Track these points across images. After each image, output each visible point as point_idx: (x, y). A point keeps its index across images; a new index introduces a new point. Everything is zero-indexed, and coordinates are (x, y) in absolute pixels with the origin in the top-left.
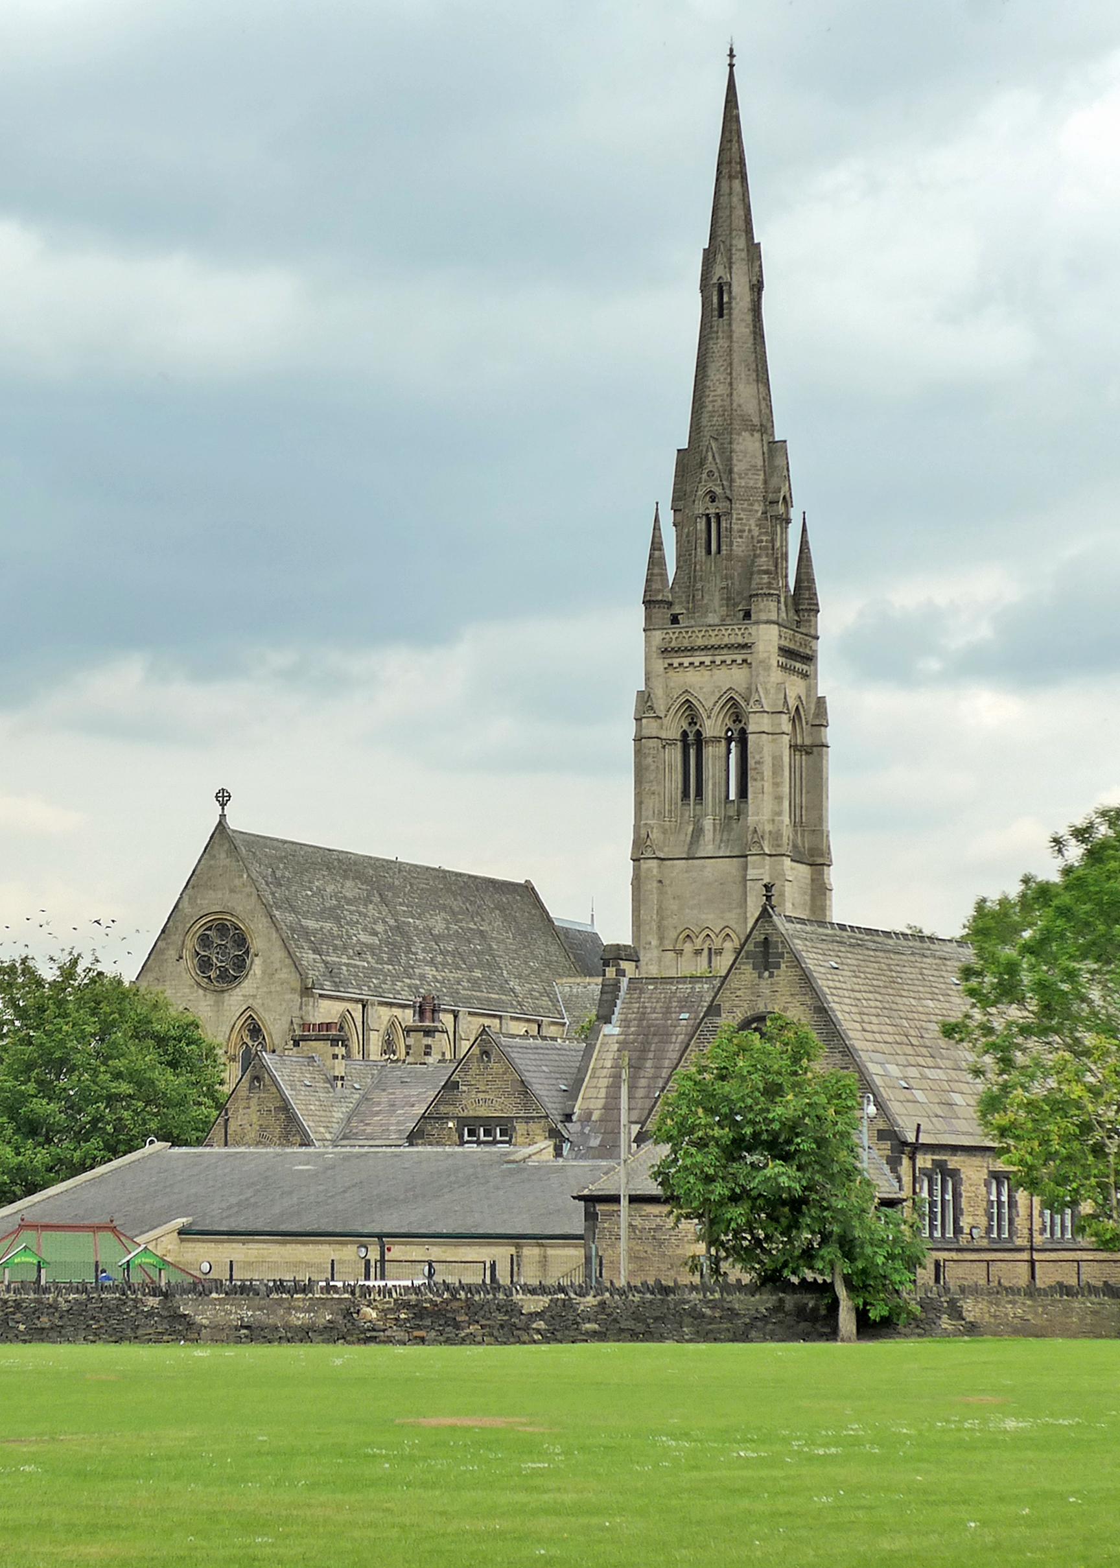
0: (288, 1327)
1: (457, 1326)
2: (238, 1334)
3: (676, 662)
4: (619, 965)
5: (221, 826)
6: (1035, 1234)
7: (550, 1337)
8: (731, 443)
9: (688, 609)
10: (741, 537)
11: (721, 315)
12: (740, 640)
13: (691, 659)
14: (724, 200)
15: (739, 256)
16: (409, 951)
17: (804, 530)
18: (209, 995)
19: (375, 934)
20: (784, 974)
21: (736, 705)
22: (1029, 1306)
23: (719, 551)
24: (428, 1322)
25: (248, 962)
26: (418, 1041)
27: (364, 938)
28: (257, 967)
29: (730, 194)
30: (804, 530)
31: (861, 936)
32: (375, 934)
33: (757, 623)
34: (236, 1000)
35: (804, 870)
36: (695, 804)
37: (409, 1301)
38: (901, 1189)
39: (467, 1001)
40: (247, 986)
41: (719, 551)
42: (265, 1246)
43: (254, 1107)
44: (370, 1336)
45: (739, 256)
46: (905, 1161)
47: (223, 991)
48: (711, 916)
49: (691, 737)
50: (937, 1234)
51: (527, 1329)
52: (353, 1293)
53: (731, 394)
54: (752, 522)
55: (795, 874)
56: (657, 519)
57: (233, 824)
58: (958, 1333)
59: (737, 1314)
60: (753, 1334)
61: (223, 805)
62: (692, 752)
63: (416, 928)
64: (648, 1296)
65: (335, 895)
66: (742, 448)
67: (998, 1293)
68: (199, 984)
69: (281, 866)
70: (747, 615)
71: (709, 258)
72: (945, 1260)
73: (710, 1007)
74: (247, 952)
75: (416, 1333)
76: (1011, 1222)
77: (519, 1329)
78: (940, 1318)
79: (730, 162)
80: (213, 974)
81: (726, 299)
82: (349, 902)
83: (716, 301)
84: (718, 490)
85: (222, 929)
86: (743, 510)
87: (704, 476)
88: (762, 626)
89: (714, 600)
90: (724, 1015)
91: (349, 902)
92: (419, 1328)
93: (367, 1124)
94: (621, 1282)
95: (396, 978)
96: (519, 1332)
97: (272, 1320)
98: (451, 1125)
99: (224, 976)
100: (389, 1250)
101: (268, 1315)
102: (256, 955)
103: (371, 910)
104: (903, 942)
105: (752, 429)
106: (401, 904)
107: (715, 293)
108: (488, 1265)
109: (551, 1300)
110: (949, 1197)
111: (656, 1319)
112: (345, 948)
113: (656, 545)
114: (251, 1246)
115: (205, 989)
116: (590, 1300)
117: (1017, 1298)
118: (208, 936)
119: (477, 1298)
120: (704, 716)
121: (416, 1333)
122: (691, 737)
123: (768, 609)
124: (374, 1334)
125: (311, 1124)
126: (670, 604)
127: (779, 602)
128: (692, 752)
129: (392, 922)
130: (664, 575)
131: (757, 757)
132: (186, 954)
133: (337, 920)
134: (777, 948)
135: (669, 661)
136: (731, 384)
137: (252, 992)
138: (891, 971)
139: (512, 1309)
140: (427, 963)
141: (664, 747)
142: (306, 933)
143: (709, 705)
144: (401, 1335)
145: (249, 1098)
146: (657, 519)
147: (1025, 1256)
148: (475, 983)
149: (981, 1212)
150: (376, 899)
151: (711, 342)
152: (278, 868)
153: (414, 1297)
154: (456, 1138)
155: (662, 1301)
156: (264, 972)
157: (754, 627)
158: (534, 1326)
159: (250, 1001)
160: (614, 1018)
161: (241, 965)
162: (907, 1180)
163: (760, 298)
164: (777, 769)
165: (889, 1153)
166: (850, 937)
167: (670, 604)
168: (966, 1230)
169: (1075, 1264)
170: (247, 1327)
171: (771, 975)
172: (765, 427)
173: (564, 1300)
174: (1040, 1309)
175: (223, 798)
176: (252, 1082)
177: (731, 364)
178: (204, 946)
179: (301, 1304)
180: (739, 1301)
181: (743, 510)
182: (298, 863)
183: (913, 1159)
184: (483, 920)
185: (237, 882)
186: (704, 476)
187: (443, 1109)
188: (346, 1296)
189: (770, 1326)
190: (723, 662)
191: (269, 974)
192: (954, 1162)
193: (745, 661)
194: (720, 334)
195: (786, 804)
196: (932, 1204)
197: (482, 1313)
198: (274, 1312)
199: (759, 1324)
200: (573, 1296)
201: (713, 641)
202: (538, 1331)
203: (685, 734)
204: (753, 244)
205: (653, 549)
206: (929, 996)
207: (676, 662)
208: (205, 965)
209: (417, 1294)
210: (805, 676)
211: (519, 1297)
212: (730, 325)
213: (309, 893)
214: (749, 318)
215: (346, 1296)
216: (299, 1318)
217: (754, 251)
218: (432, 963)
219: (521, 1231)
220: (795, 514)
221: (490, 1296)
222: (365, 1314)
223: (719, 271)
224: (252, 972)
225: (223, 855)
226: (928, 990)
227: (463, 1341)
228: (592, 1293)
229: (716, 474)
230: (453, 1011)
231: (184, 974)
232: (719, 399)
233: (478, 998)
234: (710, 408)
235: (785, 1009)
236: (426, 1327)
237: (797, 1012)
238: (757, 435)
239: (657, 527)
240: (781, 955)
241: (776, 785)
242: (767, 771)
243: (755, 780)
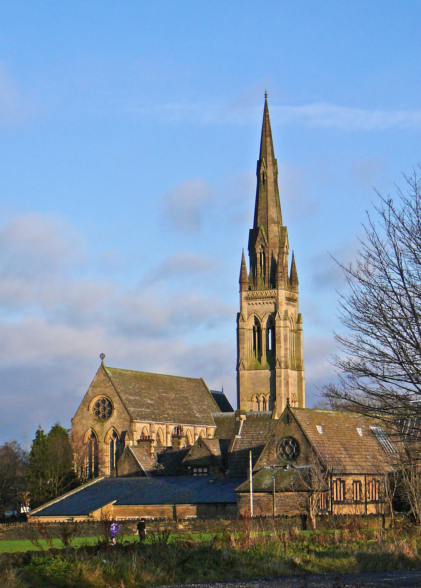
3: (250, 303)
4: (240, 416)
5: (102, 366)
6: (367, 499)
13: (256, 302)
14: (264, 144)
15: (270, 162)
16: (163, 406)
17: (293, 256)
20: (293, 424)
27: (149, 401)
28: (115, 413)
30: (293, 256)
32: (153, 400)
34: (108, 424)
35: (295, 373)
40: (112, 420)
45: (270, 162)
48: (264, 390)
55: (293, 374)
56: (243, 254)
57: (105, 365)
61: (102, 359)
63: (165, 396)
71: (259, 163)
76: (360, 496)
81: (265, 178)
83: (261, 180)
94: (126, 472)
105: (275, 223)
113: (243, 263)
115: (97, 421)
123: (282, 284)
127: (285, 282)
130: (246, 273)
131: (279, 335)
135: (248, 302)
137: (113, 421)
142: (130, 401)
146: (243, 254)
160: (239, 433)
161: (110, 413)
163: (277, 177)
164: (285, 340)
171: (289, 425)
172: (279, 223)
175: (102, 356)
183: (331, 478)
185: (107, 385)
191: (119, 417)
192: (343, 478)
195: (288, 351)
203: (254, 327)
204: (274, 159)
205: (242, 264)
208: (98, 413)
210: (294, 306)
214: (273, 184)
217: (275, 163)
218: (171, 409)
220: (290, 252)
223: (262, 169)
235: (294, 435)
237: (297, 436)
238: (277, 225)
239: (243, 257)
241: (285, 344)
242: (282, 341)
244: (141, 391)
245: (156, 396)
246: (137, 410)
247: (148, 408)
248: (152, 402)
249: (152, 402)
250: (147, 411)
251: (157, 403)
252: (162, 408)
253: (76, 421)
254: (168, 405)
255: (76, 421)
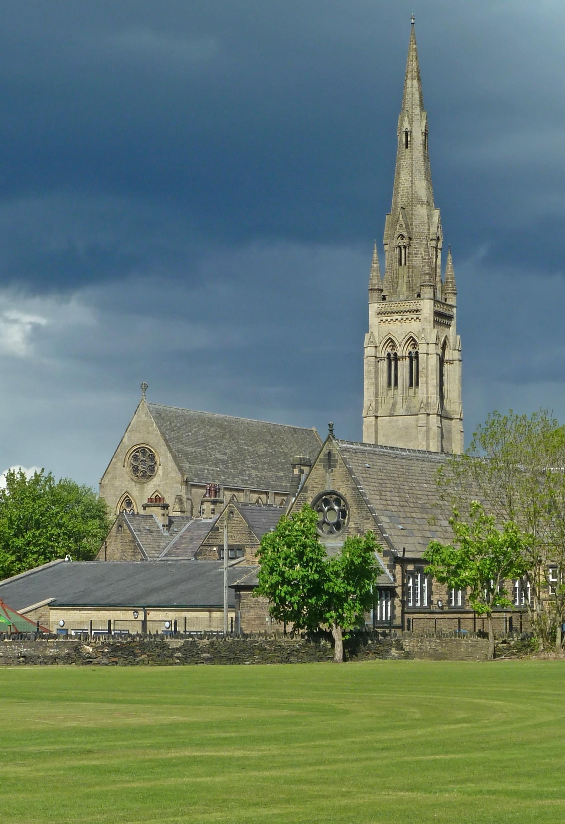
0: (45, 657)
1: (135, 655)
2: (18, 660)
7: (184, 661)
8: (412, 210)
9: (390, 293)
10: (416, 257)
11: (407, 147)
12: (415, 308)
13: (391, 318)
18: (138, 485)
19: (226, 454)
20: (339, 470)
21: (414, 340)
22: (438, 643)
23: (405, 264)
24: (119, 653)
25: (156, 468)
26: (208, 507)
28: (160, 471)
29: (412, 87)
31: (387, 451)
32: (226, 454)
33: (423, 299)
34: (150, 489)
36: (394, 389)
37: (109, 643)
38: (395, 580)
39: (273, 487)
41: (405, 264)
42: (89, 612)
43: (119, 541)
44: (88, 661)
46: (398, 568)
47: (144, 483)
49: (392, 356)
50: (418, 604)
51: (171, 656)
52: (80, 639)
53: (412, 186)
54: (422, 250)
58: (400, 658)
59: (284, 648)
60: (292, 658)
62: (393, 364)
63: (249, 451)
64: (236, 639)
65: (204, 435)
66: (417, 213)
67: (422, 636)
68: (132, 479)
69: (175, 421)
70: (419, 295)
72: (413, 619)
73: (302, 488)
74: (156, 463)
75: (113, 659)
77: (168, 657)
78: (391, 649)
79: (412, 71)
80: (139, 475)
81: (409, 139)
82: (212, 438)
84: (405, 234)
85: (143, 451)
86: (417, 243)
87: (398, 227)
88: (425, 301)
89: (403, 288)
90: (309, 492)
91: (212, 438)
92: (114, 656)
93: (177, 549)
95: (234, 476)
96: (167, 659)
97: (37, 653)
98: (215, 549)
99: (144, 476)
100: (149, 614)
101: (34, 650)
102: (160, 465)
103: (224, 443)
104: (412, 454)
106: (241, 439)
107: (404, 136)
108: (173, 623)
109: (185, 642)
110: (425, 585)
111: (241, 651)
112: (208, 461)
114: (83, 612)
115: (135, 482)
116: (206, 641)
117: (432, 639)
118: (137, 456)
119: (145, 641)
120: (398, 345)
121: (113, 659)
122: (392, 356)
124: (91, 660)
125: (147, 549)
126: (382, 291)
128: (393, 364)
129: (236, 448)
132: (126, 464)
133: (205, 448)
134: (335, 457)
135: (381, 318)
136: (412, 181)
137: (158, 483)
138: (404, 468)
139: (164, 646)
140: (253, 468)
141: (379, 362)
142: (186, 454)
143: (400, 340)
144: (105, 660)
145: (116, 536)
147: (471, 615)
148: (279, 478)
149: (444, 592)
150: (228, 436)
151: (402, 161)
152: (173, 421)
153: (112, 640)
154: (217, 555)
155: (244, 641)
156: (163, 473)
157: (422, 301)
158: (176, 655)
159: (157, 488)
161: (152, 469)
162: (399, 577)
165: (388, 563)
166: (380, 452)
167: (382, 291)
168: (435, 602)
169: (434, 620)
170: (24, 657)
173: (192, 641)
174: (444, 645)
176: (118, 528)
177: (412, 171)
178: (136, 461)
179: (52, 644)
180: (284, 641)
181: (417, 243)
182: (185, 419)
184: (287, 447)
186: (398, 227)
187: (211, 541)
188: (76, 640)
189: (301, 654)
190: (407, 319)
193: (417, 318)
194: (406, 157)
196: (415, 589)
197: (148, 648)
198: (38, 649)
199: (295, 653)
200: (196, 639)
201: (402, 309)
202: (178, 658)
203: (389, 354)
206: (425, 482)
207: (384, 319)
208: (135, 469)
209: (113, 639)
211: (168, 640)
212: (411, 152)
213: (190, 434)
215: (76, 640)
216: (52, 652)
218: (256, 468)
219: (212, 603)
221: (153, 640)
222: (86, 649)
224: (158, 473)
225: (144, 416)
226: (425, 478)
227: (138, 663)
228: (207, 637)
229: (404, 226)
230: (266, 492)
231: (125, 474)
232: (406, 189)
233: (279, 486)
234: (402, 194)
235: (339, 489)
236: (118, 656)
240: (337, 461)
243: (422, 377)
244: (206, 441)
245: (232, 449)
246: (196, 468)
247: (216, 465)
248: (225, 457)
249: (225, 457)
250: (212, 470)
251: (231, 459)
252: (240, 467)
253: (106, 482)
254: (252, 462)
255: (106, 482)
